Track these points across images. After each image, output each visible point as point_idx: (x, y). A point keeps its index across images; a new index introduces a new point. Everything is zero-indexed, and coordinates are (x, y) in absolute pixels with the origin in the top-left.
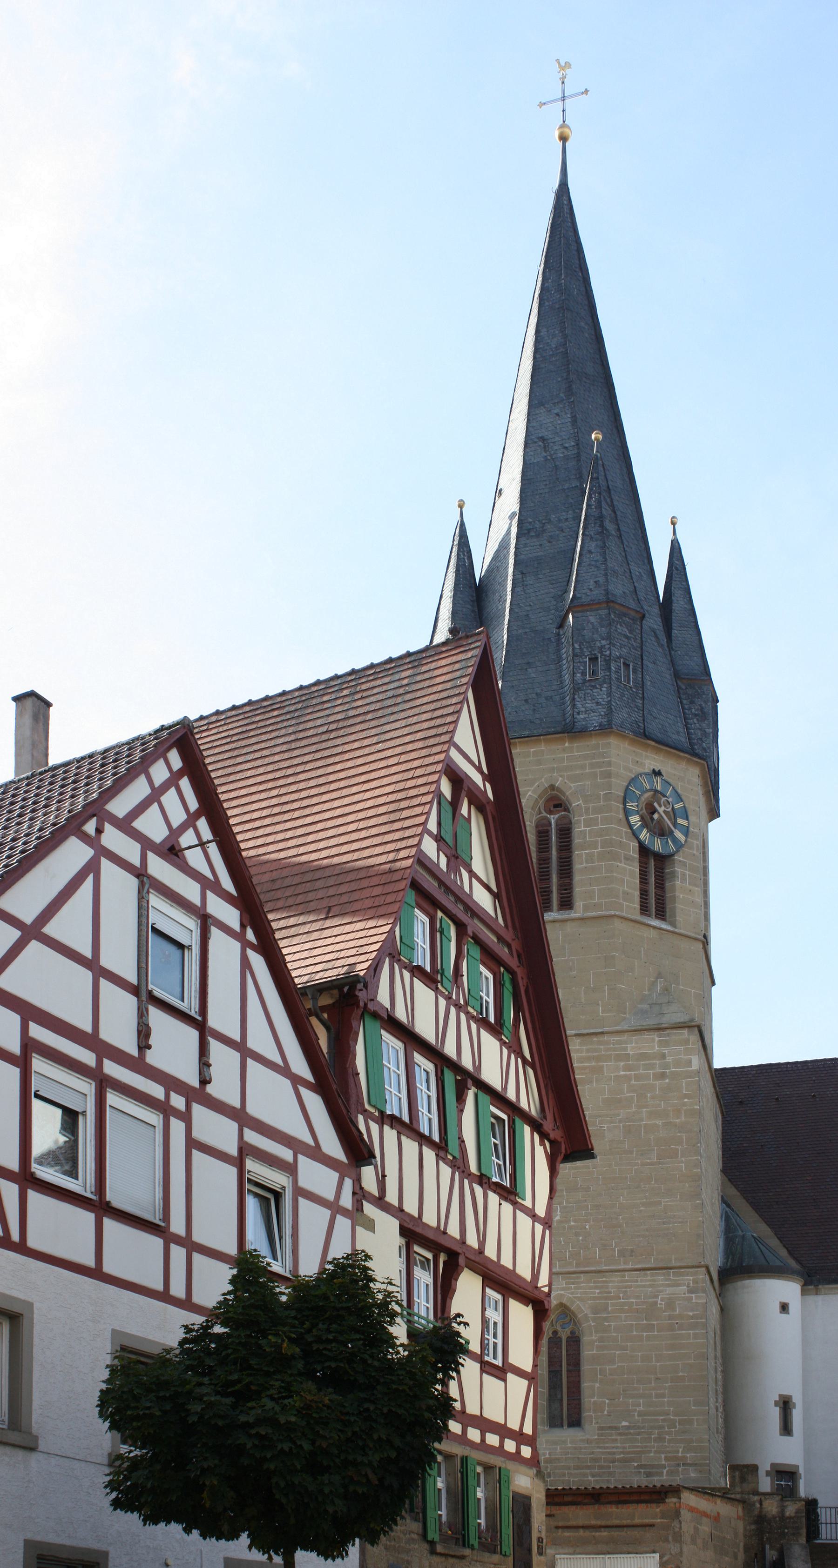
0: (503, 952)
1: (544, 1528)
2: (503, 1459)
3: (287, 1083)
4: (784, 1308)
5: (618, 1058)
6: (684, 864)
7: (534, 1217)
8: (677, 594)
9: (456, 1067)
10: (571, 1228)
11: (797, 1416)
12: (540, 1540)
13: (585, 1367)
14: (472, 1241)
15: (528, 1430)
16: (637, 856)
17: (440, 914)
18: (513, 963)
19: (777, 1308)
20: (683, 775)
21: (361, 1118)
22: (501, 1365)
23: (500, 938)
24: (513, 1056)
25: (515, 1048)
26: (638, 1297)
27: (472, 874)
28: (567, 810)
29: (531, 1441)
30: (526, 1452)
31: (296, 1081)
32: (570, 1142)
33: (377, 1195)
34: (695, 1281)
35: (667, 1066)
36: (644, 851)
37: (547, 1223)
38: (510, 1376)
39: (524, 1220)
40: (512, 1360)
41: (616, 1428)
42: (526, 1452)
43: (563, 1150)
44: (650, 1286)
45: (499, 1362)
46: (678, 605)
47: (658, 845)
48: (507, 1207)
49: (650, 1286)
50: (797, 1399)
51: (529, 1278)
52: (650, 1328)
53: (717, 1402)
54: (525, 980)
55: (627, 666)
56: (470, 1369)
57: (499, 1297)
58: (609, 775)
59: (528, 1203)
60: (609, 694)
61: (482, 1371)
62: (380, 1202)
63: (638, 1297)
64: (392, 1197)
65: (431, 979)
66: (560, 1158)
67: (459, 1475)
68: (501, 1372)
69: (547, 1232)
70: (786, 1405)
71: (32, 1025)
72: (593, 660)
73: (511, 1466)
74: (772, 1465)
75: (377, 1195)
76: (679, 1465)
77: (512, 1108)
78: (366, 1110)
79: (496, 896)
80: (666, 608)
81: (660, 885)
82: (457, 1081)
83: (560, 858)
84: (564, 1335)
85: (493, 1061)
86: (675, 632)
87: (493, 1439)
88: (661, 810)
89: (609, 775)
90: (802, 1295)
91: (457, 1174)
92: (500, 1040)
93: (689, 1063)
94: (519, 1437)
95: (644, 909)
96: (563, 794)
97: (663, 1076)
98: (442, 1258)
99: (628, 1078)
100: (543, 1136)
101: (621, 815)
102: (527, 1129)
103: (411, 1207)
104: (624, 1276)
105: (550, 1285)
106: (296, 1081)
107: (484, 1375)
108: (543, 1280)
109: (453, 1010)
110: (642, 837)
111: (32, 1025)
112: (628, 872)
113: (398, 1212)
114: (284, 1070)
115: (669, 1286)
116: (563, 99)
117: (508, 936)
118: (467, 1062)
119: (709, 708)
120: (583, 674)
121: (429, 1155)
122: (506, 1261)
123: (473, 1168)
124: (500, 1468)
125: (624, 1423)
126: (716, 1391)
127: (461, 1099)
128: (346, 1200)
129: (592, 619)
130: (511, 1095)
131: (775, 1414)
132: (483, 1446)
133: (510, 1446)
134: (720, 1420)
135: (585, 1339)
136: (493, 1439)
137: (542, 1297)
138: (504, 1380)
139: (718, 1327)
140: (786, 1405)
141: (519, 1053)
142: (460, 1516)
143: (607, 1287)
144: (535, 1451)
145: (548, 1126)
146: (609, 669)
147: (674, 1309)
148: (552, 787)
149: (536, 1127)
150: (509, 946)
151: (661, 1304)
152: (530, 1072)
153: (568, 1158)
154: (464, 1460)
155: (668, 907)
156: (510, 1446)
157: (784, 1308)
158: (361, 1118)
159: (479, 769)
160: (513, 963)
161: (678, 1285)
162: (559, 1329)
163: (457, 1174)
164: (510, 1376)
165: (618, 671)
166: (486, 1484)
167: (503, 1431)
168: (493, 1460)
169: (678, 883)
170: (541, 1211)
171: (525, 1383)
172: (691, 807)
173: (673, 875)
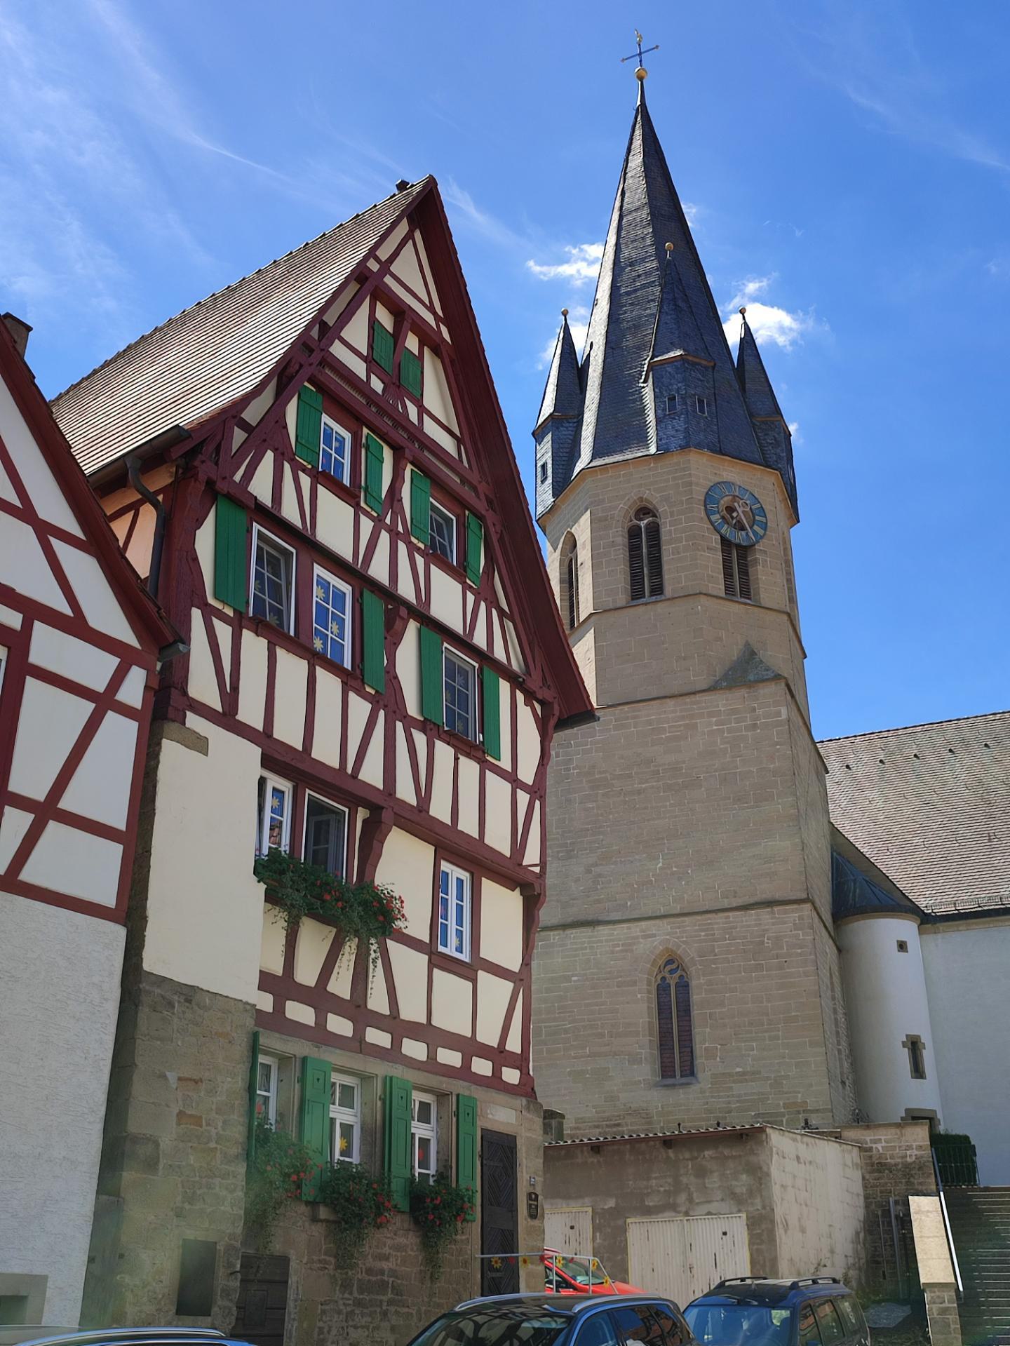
0: (466, 493)
1: (540, 1179)
2: (466, 1084)
3: (28, 531)
4: (902, 946)
5: (711, 715)
6: (765, 552)
7: (512, 777)
8: (750, 362)
9: (388, 595)
10: (673, 874)
11: (928, 1056)
12: (533, 1197)
13: (695, 1012)
14: (406, 791)
15: (514, 1044)
16: (719, 546)
17: (365, 431)
18: (481, 506)
19: (895, 946)
20: (757, 483)
21: (196, 614)
22: (467, 960)
23: (464, 481)
24: (483, 605)
25: (485, 594)
26: (745, 937)
27: (422, 410)
28: (655, 516)
29: (520, 1062)
30: (511, 1076)
31: (44, 531)
32: (563, 706)
33: (220, 710)
34: (801, 918)
35: (758, 718)
36: (726, 543)
37: (537, 791)
38: (481, 975)
39: (498, 789)
40: (485, 953)
41: (730, 1075)
42: (511, 1076)
43: (557, 713)
44: (756, 925)
45: (465, 957)
46: (750, 364)
47: (739, 537)
48: (469, 768)
49: (756, 925)
50: (926, 1039)
51: (507, 852)
52: (759, 968)
53: (839, 1043)
54: (498, 528)
55: (701, 402)
56: (409, 965)
57: (465, 876)
58: (690, 484)
59: (505, 763)
60: (686, 422)
61: (431, 965)
62: (227, 718)
63: (745, 937)
64: (250, 712)
65: (348, 495)
66: (553, 722)
67: (379, 1103)
68: (468, 970)
69: (538, 803)
70: (914, 1045)
71: (443, 863)
72: (672, 399)
73: (478, 1093)
74: (907, 1110)
75: (220, 710)
76: (799, 1112)
77: (486, 658)
78: (207, 604)
79: (459, 441)
80: (740, 371)
81: (744, 572)
82: (387, 611)
83: (649, 553)
84: (673, 981)
85: (448, 600)
86: (747, 386)
87: (449, 1057)
88: (740, 510)
89: (690, 484)
90: (920, 933)
91: (382, 713)
92: (463, 583)
93: (779, 714)
94: (499, 1055)
95: (729, 589)
96: (651, 503)
97: (754, 726)
98: (362, 814)
99: (722, 731)
100: (530, 697)
101: (703, 515)
102: (504, 687)
103: (289, 731)
104: (728, 917)
105: (543, 864)
106: (44, 531)
107: (436, 972)
108: (532, 856)
109: (385, 537)
110: (723, 531)
111: (443, 863)
112: (712, 562)
113: (263, 737)
114: (26, 513)
115: (773, 924)
116: (640, 54)
117: (475, 477)
118: (406, 589)
119: (781, 437)
120: (664, 410)
121: (329, 684)
122: (468, 824)
123: (412, 709)
124: (458, 1096)
125: (738, 1070)
126: (838, 1033)
127: (393, 640)
128: (133, 690)
129: (669, 369)
130: (480, 639)
131: (904, 1055)
132: (432, 1066)
133: (482, 1067)
134: (846, 1065)
135: (694, 983)
136: (449, 1057)
137: (531, 879)
138: (474, 981)
139: (835, 969)
140: (914, 1045)
141: (493, 603)
142: (378, 1163)
143: (713, 929)
144: (525, 1073)
145: (534, 683)
146: (686, 404)
147: (782, 948)
148: (641, 499)
149: (516, 682)
150: (474, 489)
151: (768, 943)
152: (509, 625)
153: (563, 724)
154: (388, 1081)
155: (752, 587)
156: (482, 1067)
157: (902, 946)
158: (196, 614)
159: (431, 309)
160: (481, 506)
161: (785, 923)
162: (668, 976)
163: (382, 713)
164: (481, 975)
165: (693, 405)
166: (439, 1118)
167: (469, 1047)
168: (459, 1087)
169: (760, 568)
170: (527, 774)
171: (509, 986)
172: (767, 507)
173: (756, 561)
